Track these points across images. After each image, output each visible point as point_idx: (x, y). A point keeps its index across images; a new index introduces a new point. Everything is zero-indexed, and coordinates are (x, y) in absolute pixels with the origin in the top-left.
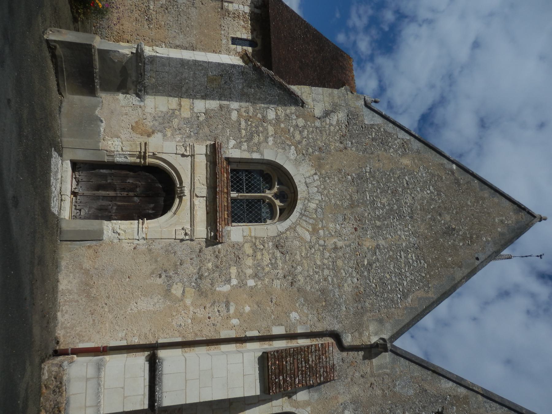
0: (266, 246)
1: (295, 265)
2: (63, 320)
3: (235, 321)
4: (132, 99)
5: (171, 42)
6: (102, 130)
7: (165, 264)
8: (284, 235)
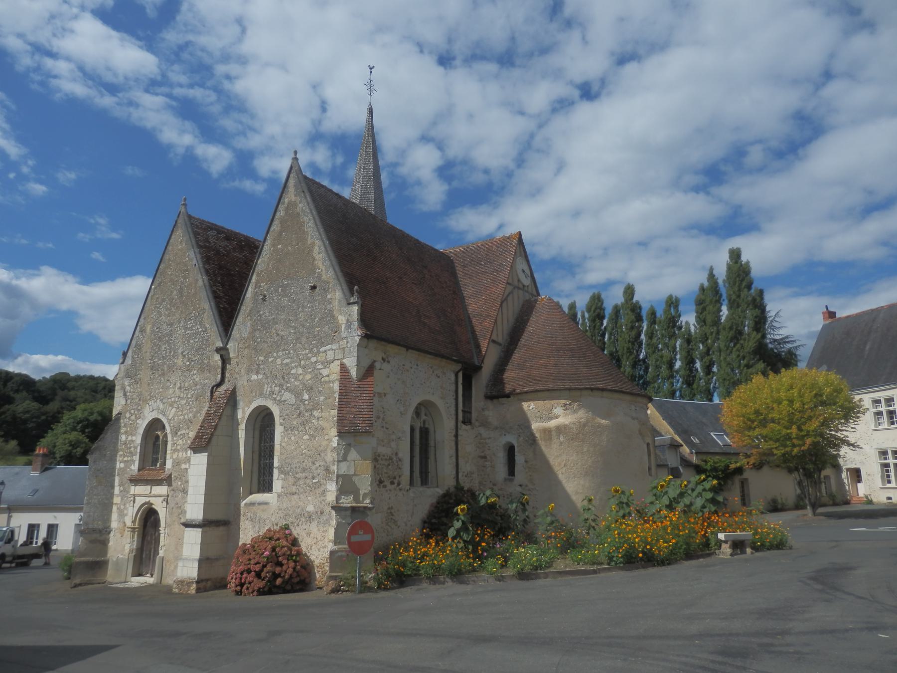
4: (112, 534)
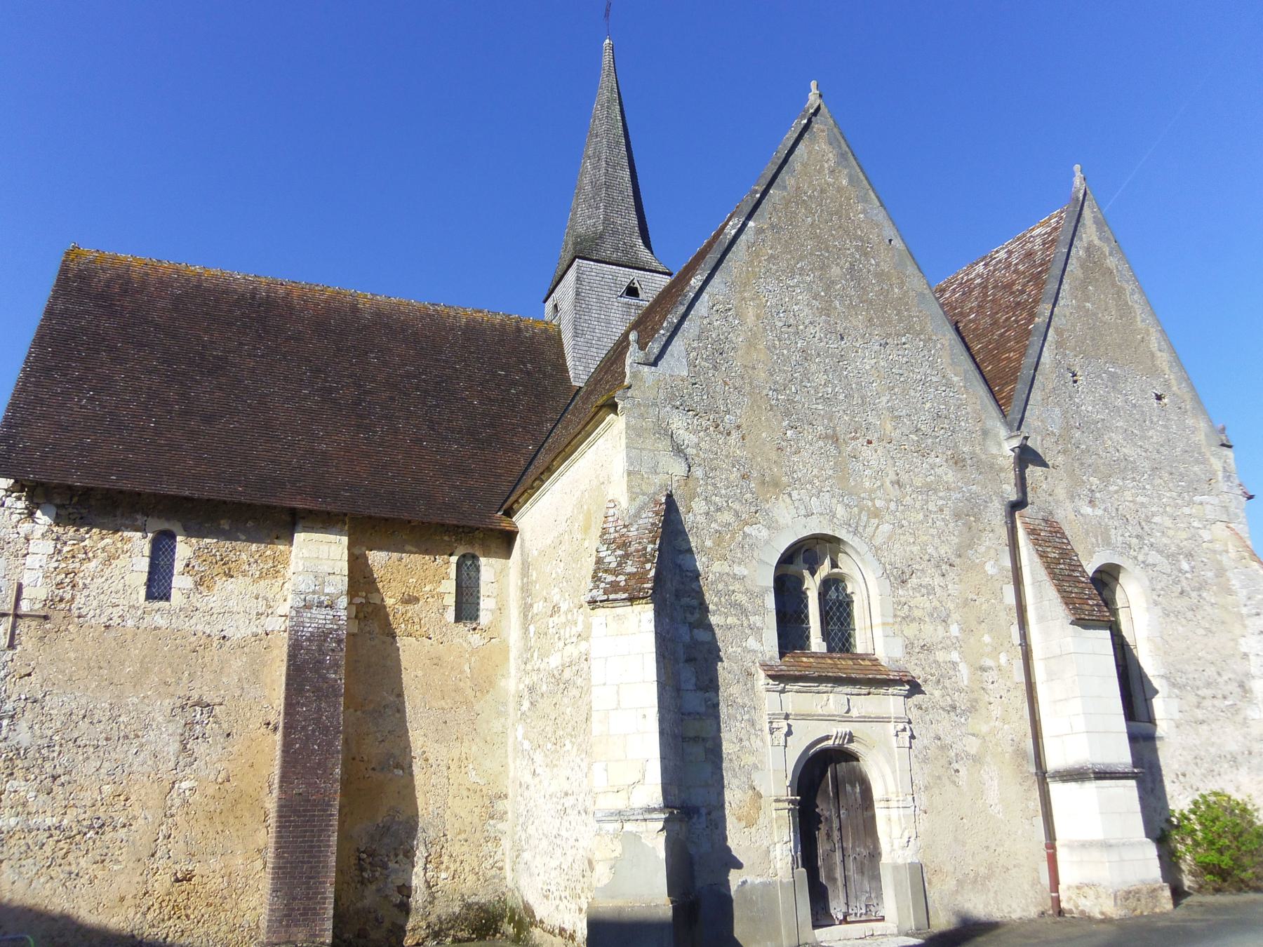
0: (903, 600)
1: (927, 557)
2: (1019, 910)
3: (1003, 659)
5: (172, 765)
6: (758, 880)
7: (940, 765)
8: (888, 567)
